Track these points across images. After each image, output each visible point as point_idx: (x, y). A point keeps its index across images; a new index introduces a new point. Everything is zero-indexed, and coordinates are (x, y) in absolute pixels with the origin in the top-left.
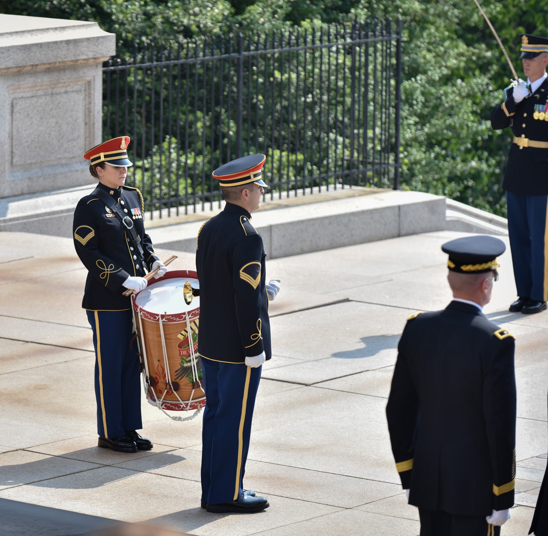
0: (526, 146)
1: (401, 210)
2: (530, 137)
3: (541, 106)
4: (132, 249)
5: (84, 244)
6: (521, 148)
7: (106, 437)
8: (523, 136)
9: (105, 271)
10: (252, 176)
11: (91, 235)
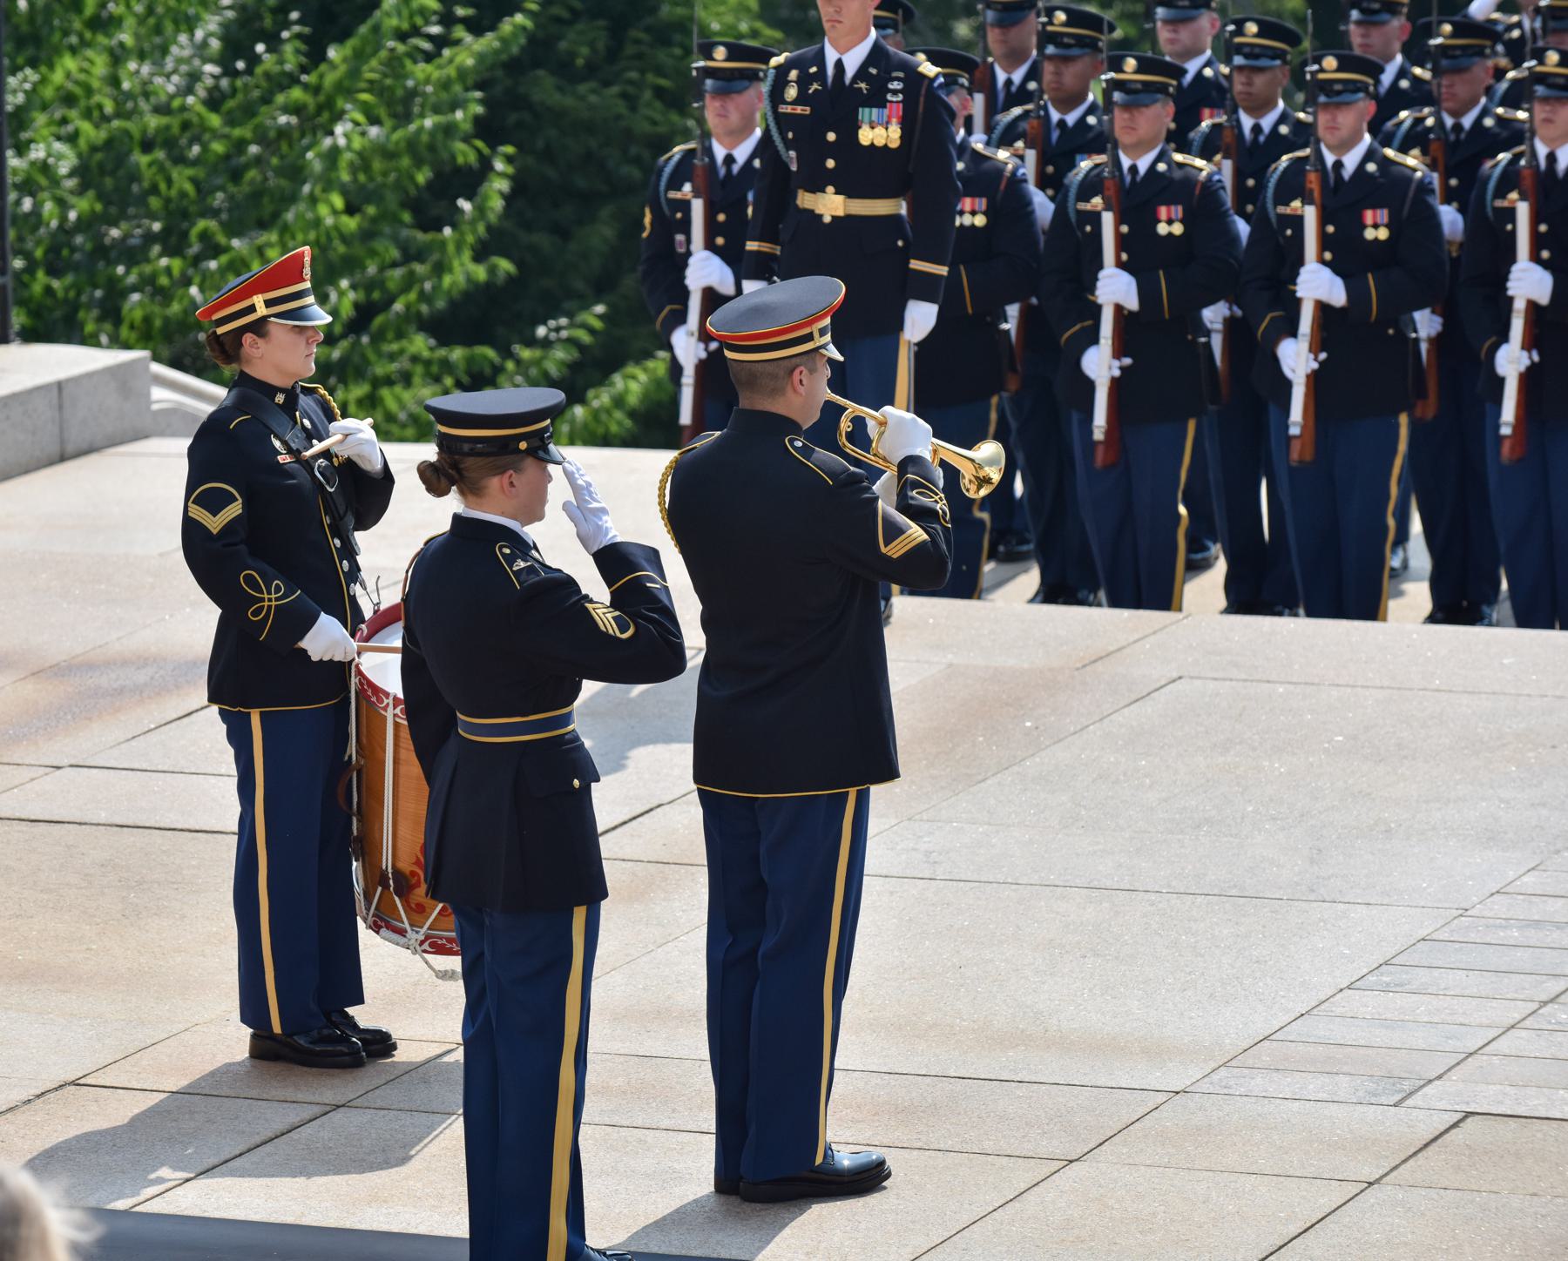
0: (841, 213)
1: (65, 393)
3: (875, 110)
4: (337, 542)
5: (215, 532)
6: (827, 219)
8: (830, 189)
9: (263, 600)
10: (816, 335)
11: (234, 510)
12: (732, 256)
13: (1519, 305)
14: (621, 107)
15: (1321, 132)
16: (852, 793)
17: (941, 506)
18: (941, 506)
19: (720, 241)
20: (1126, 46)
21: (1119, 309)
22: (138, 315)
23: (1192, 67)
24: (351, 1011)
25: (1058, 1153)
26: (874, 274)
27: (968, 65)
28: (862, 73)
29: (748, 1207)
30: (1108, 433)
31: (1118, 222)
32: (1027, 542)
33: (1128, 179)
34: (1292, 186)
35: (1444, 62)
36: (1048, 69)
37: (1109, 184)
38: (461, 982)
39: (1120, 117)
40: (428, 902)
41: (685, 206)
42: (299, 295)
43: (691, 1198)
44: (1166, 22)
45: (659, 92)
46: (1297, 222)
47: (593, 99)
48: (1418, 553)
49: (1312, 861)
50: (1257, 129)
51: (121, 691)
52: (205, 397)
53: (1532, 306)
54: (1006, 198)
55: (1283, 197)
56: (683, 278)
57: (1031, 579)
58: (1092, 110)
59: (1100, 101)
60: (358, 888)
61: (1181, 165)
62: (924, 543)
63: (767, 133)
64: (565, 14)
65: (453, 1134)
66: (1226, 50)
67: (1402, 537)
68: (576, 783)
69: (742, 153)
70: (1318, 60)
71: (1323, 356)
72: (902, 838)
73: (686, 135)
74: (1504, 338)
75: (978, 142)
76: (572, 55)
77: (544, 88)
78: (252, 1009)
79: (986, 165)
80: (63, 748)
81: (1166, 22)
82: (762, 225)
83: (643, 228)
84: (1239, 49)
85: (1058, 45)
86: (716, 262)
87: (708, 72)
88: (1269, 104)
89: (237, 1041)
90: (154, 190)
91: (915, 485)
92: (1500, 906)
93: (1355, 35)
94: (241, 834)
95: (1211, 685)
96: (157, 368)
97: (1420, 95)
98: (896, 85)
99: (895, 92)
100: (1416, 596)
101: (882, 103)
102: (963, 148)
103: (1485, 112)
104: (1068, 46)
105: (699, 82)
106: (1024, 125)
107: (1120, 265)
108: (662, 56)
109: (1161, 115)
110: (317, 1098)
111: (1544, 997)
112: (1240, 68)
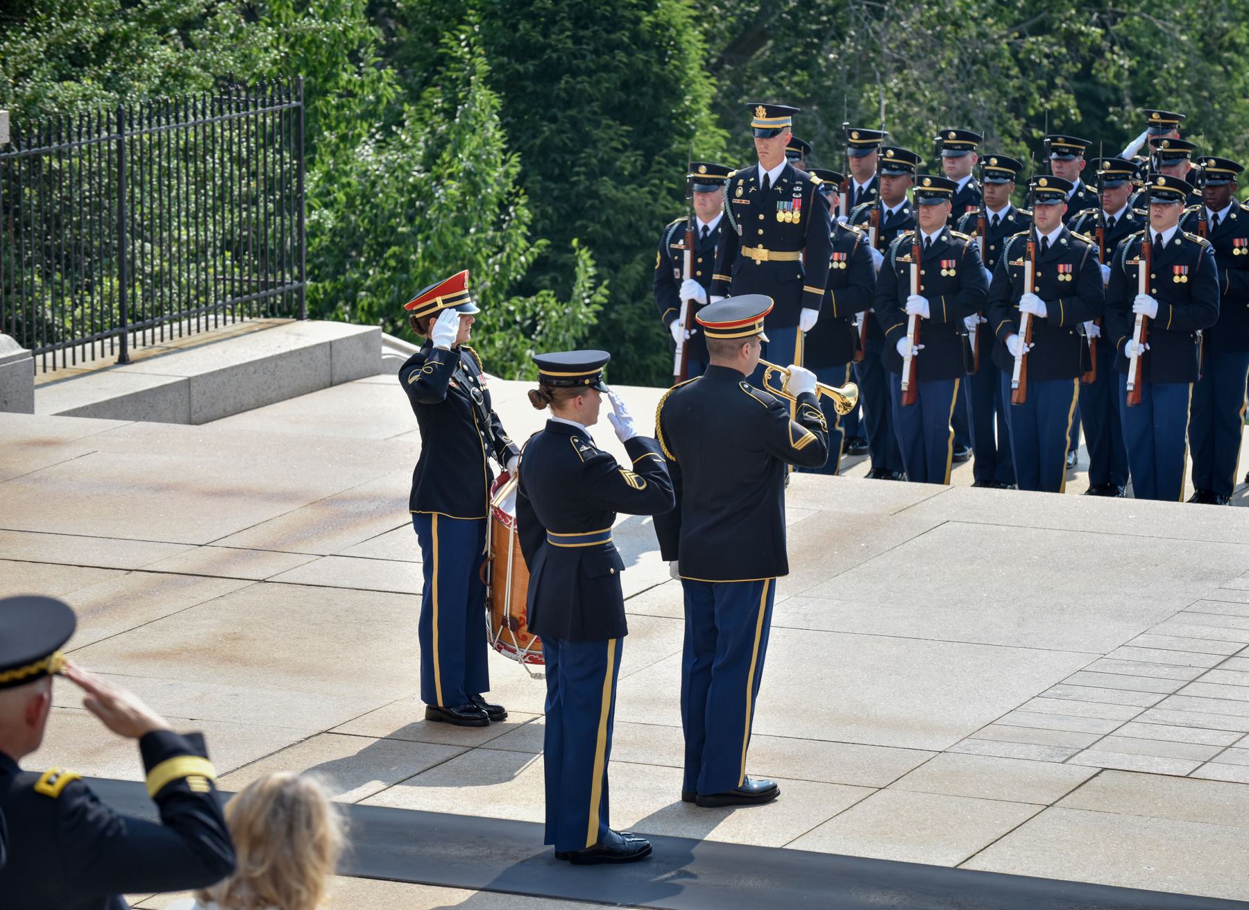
2: (770, 246)
6: (758, 263)
7: (440, 704)
8: (760, 246)
12: (705, 282)
13: (1139, 318)
14: (649, 199)
15: (1036, 221)
16: (767, 580)
17: (822, 420)
18: (822, 420)
19: (699, 273)
20: (925, 171)
21: (918, 317)
22: (365, 303)
23: (962, 183)
24: (482, 695)
25: (873, 784)
26: (786, 290)
27: (838, 179)
28: (779, 182)
29: (700, 809)
30: (909, 387)
31: (920, 268)
32: (865, 444)
33: (701, 235)
34: (1019, 250)
35: (1105, 183)
36: (883, 182)
37: (914, 248)
38: (544, 681)
39: (922, 211)
40: (528, 634)
41: (680, 253)
42: (461, 297)
43: (669, 804)
44: (948, 157)
45: (670, 191)
46: (1021, 270)
47: (633, 194)
48: (1083, 455)
49: (1019, 626)
50: (996, 217)
51: (360, 514)
52: (405, 350)
53: (1146, 318)
54: (858, 254)
55: (1013, 256)
56: (678, 293)
57: (866, 465)
58: (907, 205)
59: (911, 201)
60: (489, 628)
61: (955, 238)
62: (814, 442)
63: (725, 213)
64: (620, 147)
65: (538, 763)
66: (982, 174)
68: (612, 570)
69: (712, 225)
70: (1037, 180)
71: (1032, 345)
72: (790, 606)
73: (684, 214)
74: (1130, 336)
75: (842, 221)
76: (623, 169)
78: (428, 693)
79: (847, 235)
80: (326, 545)
81: (948, 157)
82: (722, 263)
83: (655, 263)
84: (987, 173)
85: (889, 169)
86: (697, 285)
87: (696, 180)
88: (1003, 204)
89: (419, 710)
91: (807, 409)
92: (1124, 653)
93: (1055, 167)
94: (424, 595)
95: (965, 525)
96: (385, 336)
97: (1091, 201)
98: (798, 189)
99: (797, 193)
100: (1083, 479)
101: (790, 199)
102: (834, 224)
103: (1127, 211)
104: (895, 170)
105: (691, 185)
106: (868, 213)
107: (920, 293)
108: (672, 171)
109: (944, 209)
110: (462, 743)
111: (1173, 697)
112: (988, 184)
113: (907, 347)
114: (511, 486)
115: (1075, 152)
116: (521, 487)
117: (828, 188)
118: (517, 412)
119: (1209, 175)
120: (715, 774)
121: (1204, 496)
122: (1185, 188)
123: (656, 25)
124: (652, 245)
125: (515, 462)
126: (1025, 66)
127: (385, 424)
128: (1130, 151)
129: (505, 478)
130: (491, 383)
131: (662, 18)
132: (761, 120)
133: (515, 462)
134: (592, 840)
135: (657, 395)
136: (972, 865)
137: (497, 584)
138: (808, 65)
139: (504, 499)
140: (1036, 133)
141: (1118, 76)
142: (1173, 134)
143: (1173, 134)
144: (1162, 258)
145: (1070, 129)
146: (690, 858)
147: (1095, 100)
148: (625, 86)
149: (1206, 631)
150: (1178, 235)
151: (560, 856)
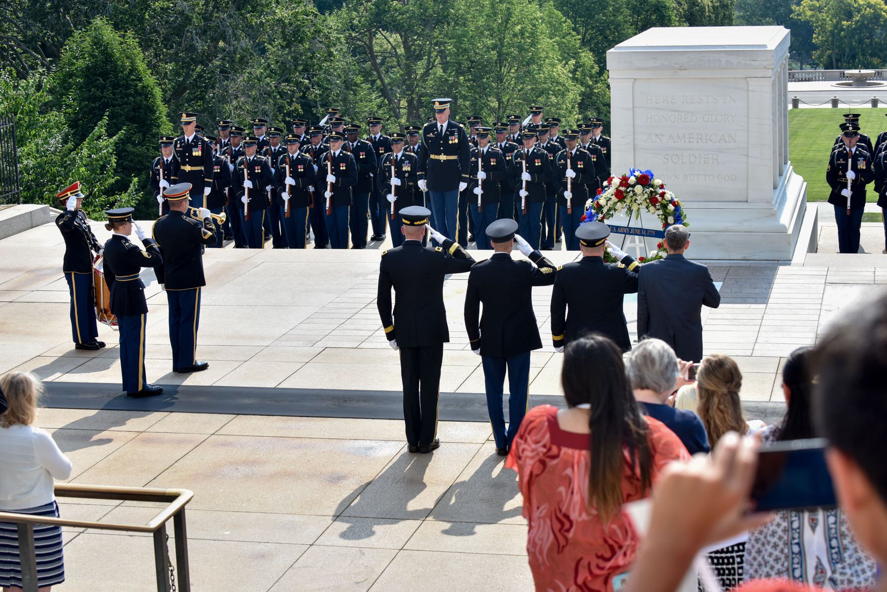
2: (191, 165)
12: (168, 180)
17: (214, 227)
18: (214, 227)
27: (214, 139)
28: (193, 141)
34: (283, 161)
41: (158, 170)
47: (140, 149)
48: (312, 235)
54: (224, 166)
55: (282, 163)
57: (233, 244)
65: (118, 362)
66: (268, 134)
67: (309, 232)
69: (170, 159)
72: (208, 297)
77: (130, 147)
80: (34, 287)
82: (174, 173)
89: (73, 346)
90: (48, 171)
92: (331, 305)
100: (313, 243)
109: (255, 148)
113: (245, 199)
114: (100, 260)
115: (302, 124)
116: (104, 260)
117: (211, 142)
118: (101, 233)
119: (349, 130)
120: (184, 359)
121: (356, 247)
122: (343, 135)
123: (143, 87)
124: (148, 168)
125: (101, 251)
126: (282, 94)
127: (50, 242)
128: (322, 123)
129: (98, 257)
130: (91, 223)
131: (145, 84)
132: (184, 118)
133: (101, 251)
134: (140, 388)
135: (151, 223)
136: (280, 386)
137: (98, 297)
138: (202, 98)
139: (98, 266)
140: (287, 119)
141: (316, 97)
142: (337, 116)
143: (337, 116)
144: (336, 161)
145: (301, 118)
146: (176, 392)
147: (307, 105)
148: (134, 110)
149: (360, 295)
150: (341, 152)
151: (129, 395)
